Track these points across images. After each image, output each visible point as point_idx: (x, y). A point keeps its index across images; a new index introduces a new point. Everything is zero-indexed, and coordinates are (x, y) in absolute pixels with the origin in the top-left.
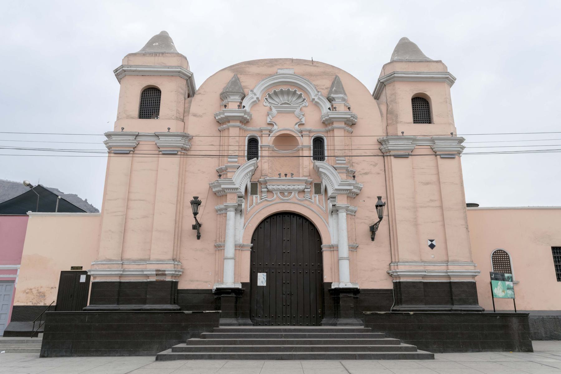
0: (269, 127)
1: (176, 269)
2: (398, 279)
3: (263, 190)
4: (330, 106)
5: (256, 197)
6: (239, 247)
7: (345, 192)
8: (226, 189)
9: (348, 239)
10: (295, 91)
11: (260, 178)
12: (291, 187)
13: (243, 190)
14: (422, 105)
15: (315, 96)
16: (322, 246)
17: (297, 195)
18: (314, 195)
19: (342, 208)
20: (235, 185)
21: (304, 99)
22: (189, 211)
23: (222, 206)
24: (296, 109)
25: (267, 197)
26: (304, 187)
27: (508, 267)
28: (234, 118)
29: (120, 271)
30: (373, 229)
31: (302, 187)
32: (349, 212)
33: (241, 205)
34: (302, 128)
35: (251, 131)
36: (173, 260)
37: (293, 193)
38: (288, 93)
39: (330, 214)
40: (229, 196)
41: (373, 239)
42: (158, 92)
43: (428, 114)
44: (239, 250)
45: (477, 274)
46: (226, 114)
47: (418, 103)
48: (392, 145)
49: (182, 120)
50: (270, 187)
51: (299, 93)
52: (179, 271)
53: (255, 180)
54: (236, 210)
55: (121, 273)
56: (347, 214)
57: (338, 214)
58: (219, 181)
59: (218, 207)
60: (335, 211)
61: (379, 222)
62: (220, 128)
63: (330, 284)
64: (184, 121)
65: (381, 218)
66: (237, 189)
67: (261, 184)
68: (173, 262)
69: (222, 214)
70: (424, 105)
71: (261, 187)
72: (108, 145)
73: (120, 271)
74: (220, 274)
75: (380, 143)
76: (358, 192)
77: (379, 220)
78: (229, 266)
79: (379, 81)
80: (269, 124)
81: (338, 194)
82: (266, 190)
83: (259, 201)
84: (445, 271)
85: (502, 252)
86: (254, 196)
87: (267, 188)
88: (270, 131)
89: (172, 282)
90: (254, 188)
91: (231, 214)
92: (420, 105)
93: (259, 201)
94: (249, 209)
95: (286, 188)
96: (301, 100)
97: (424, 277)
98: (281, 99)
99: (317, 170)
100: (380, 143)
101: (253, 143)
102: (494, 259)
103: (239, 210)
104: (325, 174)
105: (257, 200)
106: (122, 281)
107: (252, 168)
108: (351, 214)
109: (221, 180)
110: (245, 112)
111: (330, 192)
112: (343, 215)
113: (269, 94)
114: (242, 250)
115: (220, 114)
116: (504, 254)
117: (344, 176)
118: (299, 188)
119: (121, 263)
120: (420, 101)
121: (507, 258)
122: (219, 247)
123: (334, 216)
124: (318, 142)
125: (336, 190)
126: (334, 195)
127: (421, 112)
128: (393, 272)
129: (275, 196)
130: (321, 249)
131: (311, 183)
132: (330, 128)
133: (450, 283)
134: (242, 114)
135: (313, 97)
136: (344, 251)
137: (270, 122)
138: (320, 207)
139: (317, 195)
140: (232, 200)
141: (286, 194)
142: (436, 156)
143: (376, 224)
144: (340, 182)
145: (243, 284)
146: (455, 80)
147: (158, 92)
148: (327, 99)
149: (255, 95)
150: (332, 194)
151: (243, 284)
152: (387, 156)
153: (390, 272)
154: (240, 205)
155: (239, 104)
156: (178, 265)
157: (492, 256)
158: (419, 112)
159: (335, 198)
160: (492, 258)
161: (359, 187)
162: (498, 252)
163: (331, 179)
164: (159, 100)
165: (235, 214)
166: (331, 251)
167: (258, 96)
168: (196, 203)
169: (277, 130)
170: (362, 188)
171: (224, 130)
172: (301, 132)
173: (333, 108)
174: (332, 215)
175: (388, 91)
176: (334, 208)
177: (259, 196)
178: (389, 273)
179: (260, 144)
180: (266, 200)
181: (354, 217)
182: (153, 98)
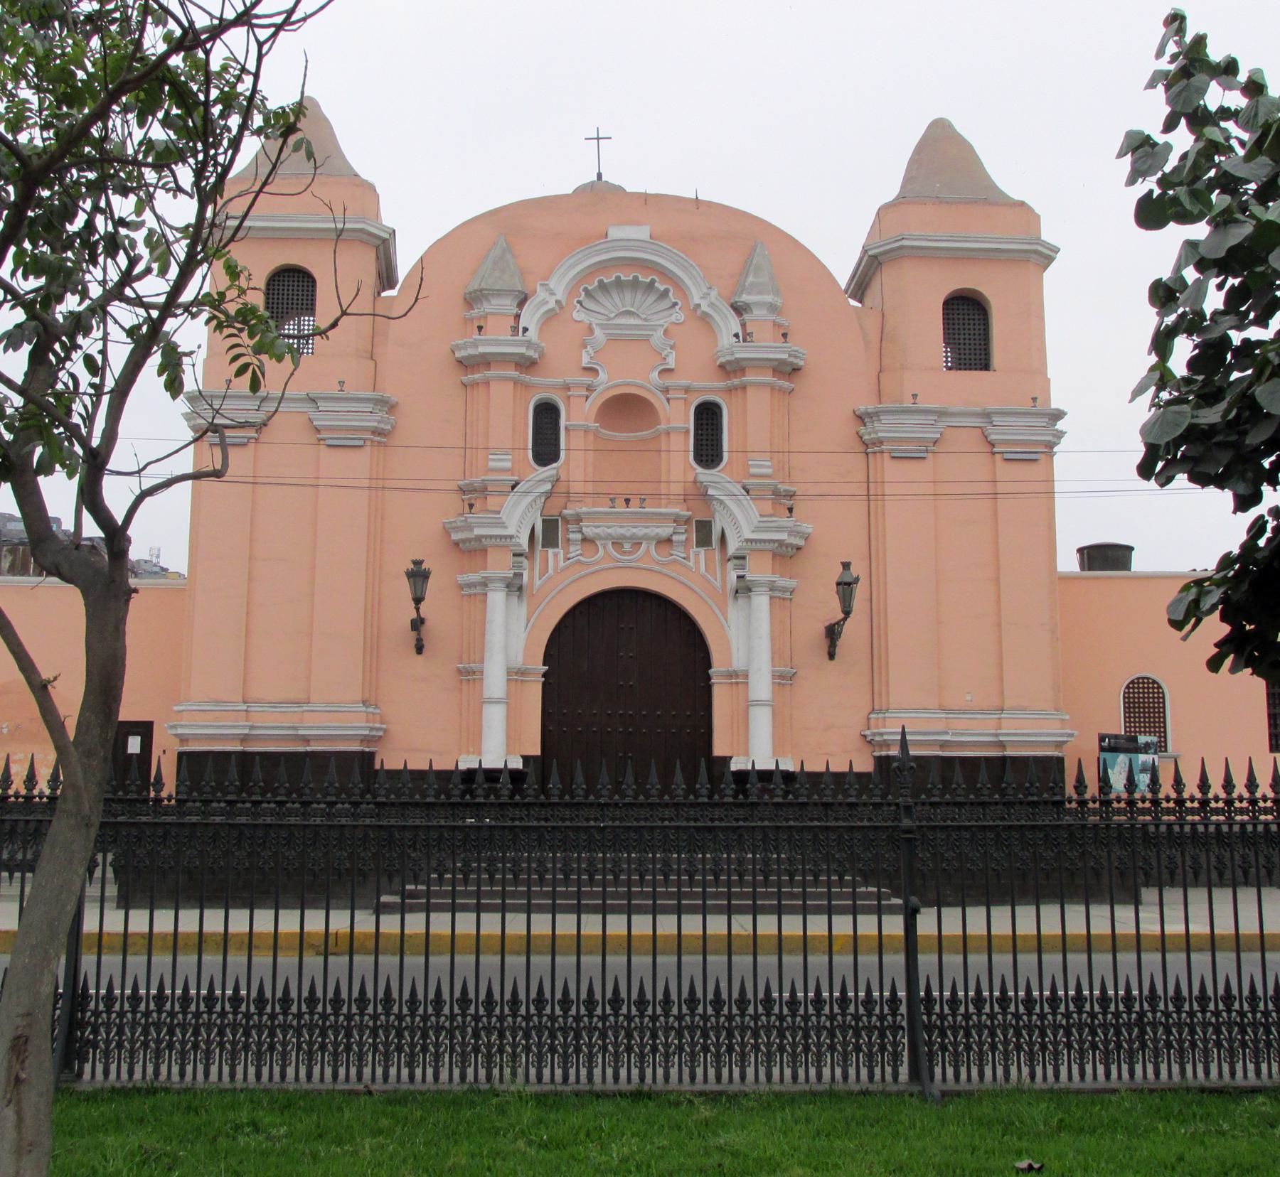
0: (587, 379)
1: (371, 725)
2: (884, 748)
3: (572, 536)
4: (736, 328)
5: (556, 555)
6: (516, 675)
7: (768, 546)
8: (486, 537)
9: (773, 659)
10: (653, 282)
11: (566, 508)
12: (640, 532)
13: (524, 541)
14: (971, 317)
15: (702, 298)
16: (711, 671)
17: (653, 549)
18: (695, 549)
19: (760, 584)
20: (506, 527)
21: (675, 304)
22: (404, 589)
23: (474, 577)
24: (655, 330)
25: (581, 555)
26: (670, 531)
27: (1159, 717)
28: (503, 359)
29: (244, 727)
30: (832, 633)
31: (665, 530)
32: (777, 594)
33: (522, 575)
34: (669, 381)
35: (545, 386)
36: (364, 702)
37: (644, 544)
38: (635, 284)
39: (732, 596)
40: (492, 557)
41: (831, 656)
42: (306, 279)
43: (983, 343)
44: (516, 680)
45: (1065, 739)
46: (482, 349)
47: (961, 312)
48: (881, 429)
49: (369, 356)
50: (589, 531)
51: (662, 288)
52: (378, 729)
53: (553, 512)
54: (508, 586)
55: (246, 731)
56: (771, 598)
57: (749, 597)
58: (469, 520)
59: (462, 578)
60: (744, 589)
61: (845, 619)
62: (464, 379)
63: (726, 760)
64: (374, 357)
65: (847, 613)
66: (511, 537)
67: (566, 521)
68: (364, 709)
69: (475, 595)
70: (976, 317)
71: (568, 530)
72: (193, 423)
73: (244, 727)
74: (474, 738)
75: (861, 418)
76: (801, 542)
77: (841, 616)
78: (495, 718)
79: (865, 251)
80: (585, 369)
81: (752, 550)
82: (579, 536)
83: (562, 564)
84: (994, 731)
85: (1148, 683)
86: (551, 551)
87: (581, 531)
88: (590, 389)
89: (363, 753)
90: (550, 532)
91: (497, 599)
92: (966, 317)
93: (562, 564)
94: (538, 583)
95: (628, 534)
96: (665, 304)
97: (944, 745)
98: (617, 299)
99: (701, 495)
100: (861, 418)
101: (547, 415)
102: (1129, 698)
103: (515, 587)
104: (721, 502)
105: (556, 563)
106: (249, 749)
107: (548, 487)
108: (781, 598)
109: (472, 518)
110: (529, 344)
111: (733, 547)
112: (761, 601)
113: (586, 290)
114: (522, 681)
115: (465, 347)
116: (1153, 688)
117: (767, 506)
118: (657, 534)
119: (245, 708)
120: (966, 307)
121: (1158, 698)
122: (470, 675)
123: (742, 601)
124: (708, 417)
125: (747, 541)
126: (741, 553)
127: (967, 336)
128: (874, 734)
129: (601, 551)
130: (709, 678)
131: (688, 521)
132: (736, 381)
133: (1004, 758)
134: (522, 350)
135: (697, 301)
136: (761, 686)
137: (590, 363)
138: (708, 581)
139: (702, 551)
140: (499, 565)
141: (627, 547)
142: (994, 454)
143: (838, 623)
144: (756, 523)
145: (526, 759)
146: (1057, 252)
147: (306, 279)
148: (732, 306)
149: (552, 294)
150: (737, 549)
151: (526, 759)
152: (874, 453)
153: (868, 732)
154: (519, 576)
155: (511, 322)
156: (374, 714)
157: (1125, 693)
158: (962, 336)
159: (743, 558)
160: (1124, 697)
161: (803, 533)
162: (1138, 683)
163: (737, 515)
164: (310, 298)
165: (507, 595)
166: (732, 683)
167: (559, 296)
168: (418, 575)
169: (607, 382)
170: (809, 534)
171: (475, 384)
172: (666, 390)
173: (745, 336)
174: (736, 598)
175: (886, 281)
176: (742, 584)
177: (562, 552)
178: (865, 736)
179: (563, 422)
180: (579, 562)
181: (788, 603)
182: (295, 297)
